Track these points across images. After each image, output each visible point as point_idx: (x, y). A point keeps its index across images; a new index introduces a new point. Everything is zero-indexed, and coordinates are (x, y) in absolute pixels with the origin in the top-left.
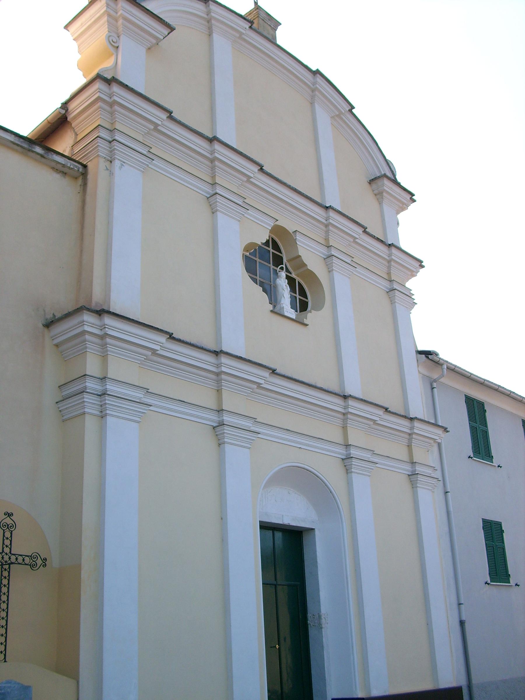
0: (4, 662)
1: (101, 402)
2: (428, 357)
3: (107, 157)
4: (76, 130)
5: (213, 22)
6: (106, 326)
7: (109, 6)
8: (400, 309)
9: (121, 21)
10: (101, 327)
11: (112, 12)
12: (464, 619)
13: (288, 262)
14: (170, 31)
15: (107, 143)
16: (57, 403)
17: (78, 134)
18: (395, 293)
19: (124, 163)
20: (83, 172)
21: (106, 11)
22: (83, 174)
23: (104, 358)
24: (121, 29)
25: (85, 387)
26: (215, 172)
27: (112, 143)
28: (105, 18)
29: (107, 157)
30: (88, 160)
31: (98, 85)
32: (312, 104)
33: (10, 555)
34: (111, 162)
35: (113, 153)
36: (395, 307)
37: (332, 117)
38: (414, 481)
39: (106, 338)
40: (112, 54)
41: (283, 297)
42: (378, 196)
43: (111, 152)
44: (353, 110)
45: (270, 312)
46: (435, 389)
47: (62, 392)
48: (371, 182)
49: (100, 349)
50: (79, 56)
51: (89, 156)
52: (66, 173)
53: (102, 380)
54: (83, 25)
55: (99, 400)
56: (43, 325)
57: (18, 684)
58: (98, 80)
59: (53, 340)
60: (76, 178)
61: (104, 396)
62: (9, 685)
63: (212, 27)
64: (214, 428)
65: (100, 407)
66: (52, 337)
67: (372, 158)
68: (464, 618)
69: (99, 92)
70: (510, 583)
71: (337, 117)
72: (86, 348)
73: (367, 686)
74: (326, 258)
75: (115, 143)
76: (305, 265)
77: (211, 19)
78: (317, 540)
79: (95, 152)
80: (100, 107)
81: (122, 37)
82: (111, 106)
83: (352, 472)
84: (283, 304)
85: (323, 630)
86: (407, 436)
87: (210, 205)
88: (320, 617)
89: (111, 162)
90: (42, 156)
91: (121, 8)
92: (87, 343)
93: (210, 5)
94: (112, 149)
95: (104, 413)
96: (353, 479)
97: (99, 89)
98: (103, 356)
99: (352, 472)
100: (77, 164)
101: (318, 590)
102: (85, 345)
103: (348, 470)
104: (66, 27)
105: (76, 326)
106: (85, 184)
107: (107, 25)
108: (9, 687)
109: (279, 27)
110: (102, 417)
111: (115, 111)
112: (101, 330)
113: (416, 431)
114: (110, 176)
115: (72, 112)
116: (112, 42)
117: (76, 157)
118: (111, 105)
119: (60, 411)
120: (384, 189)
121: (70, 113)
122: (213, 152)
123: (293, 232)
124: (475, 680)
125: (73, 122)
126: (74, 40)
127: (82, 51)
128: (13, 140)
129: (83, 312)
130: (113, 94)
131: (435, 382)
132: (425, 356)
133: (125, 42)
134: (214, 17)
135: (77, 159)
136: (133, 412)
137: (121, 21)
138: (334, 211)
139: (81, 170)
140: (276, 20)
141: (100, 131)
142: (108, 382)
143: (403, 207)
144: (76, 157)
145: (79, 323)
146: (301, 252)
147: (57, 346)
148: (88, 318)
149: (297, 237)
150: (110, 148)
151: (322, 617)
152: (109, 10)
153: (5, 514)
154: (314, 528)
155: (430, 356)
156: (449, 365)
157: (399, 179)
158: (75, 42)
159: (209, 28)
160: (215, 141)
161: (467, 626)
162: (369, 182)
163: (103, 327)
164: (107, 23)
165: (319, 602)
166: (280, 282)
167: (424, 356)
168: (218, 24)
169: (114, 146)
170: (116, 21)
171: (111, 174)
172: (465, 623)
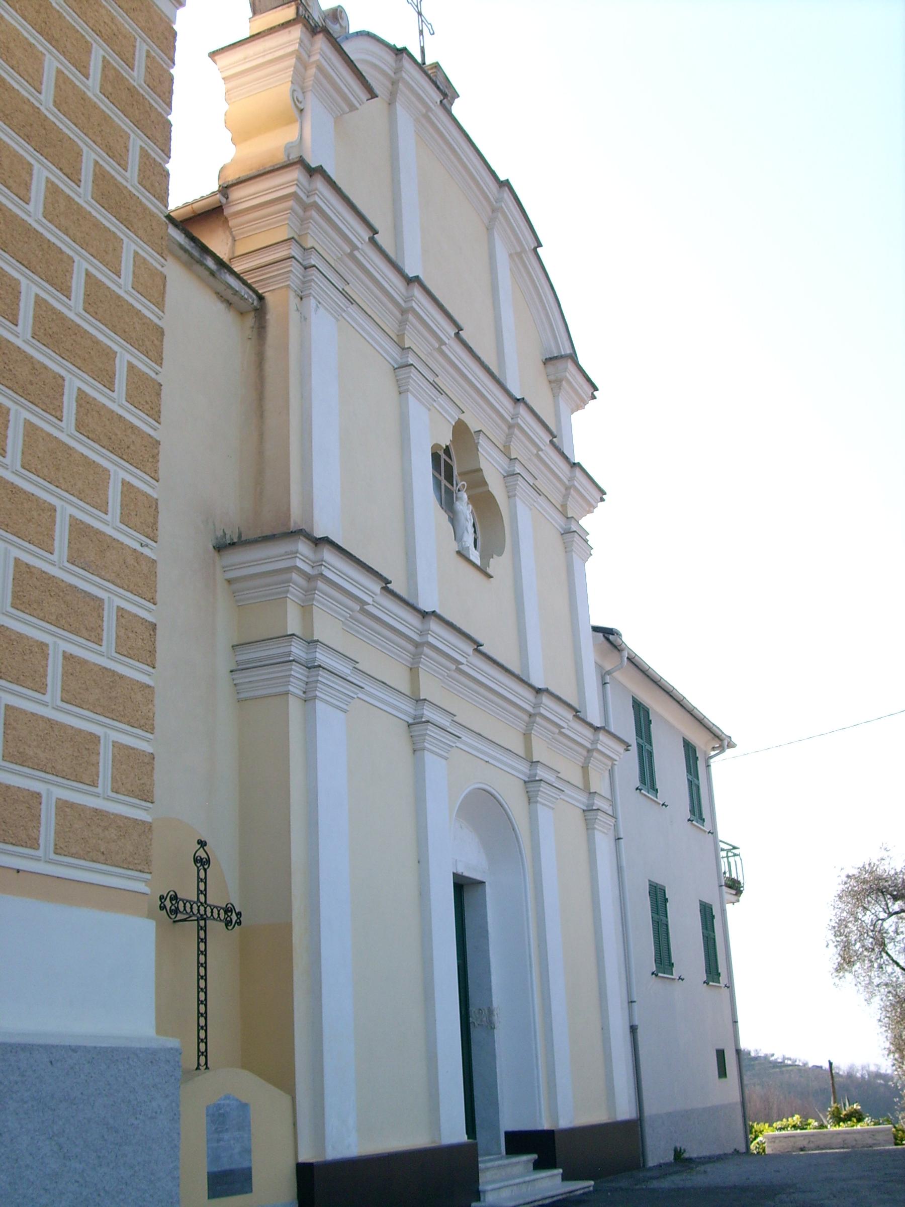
0: (205, 1069)
1: (308, 677)
2: (608, 639)
3: (298, 290)
5: (401, 85)
6: (324, 563)
7: (302, 45)
8: (576, 559)
9: (313, 71)
10: (314, 562)
11: (305, 56)
12: (637, 1024)
13: (459, 475)
14: (370, 97)
15: (300, 268)
16: (232, 671)
17: (237, 238)
18: (574, 537)
19: (320, 303)
21: (297, 50)
22: (256, 310)
23: (306, 610)
24: (309, 82)
25: (289, 654)
26: (405, 329)
27: (308, 270)
28: (293, 61)
29: (298, 290)
30: (264, 288)
31: (296, 174)
32: (489, 229)
33: (206, 906)
34: (301, 299)
35: (307, 285)
36: (572, 556)
37: (510, 255)
38: (590, 819)
39: (318, 580)
40: (297, 121)
41: (466, 532)
42: (553, 385)
43: (303, 283)
44: (539, 250)
45: (455, 553)
46: (608, 685)
47: (236, 655)
48: (548, 361)
49: (302, 595)
50: (225, 107)
51: (268, 283)
52: (230, 304)
53: (309, 643)
55: (306, 673)
56: (214, 547)
57: (237, 1100)
58: (298, 166)
59: (225, 571)
60: (242, 314)
61: (317, 669)
62: (228, 1102)
63: (397, 94)
64: (409, 725)
65: (305, 686)
66: (223, 568)
67: (551, 325)
68: (636, 1022)
69: (297, 184)
70: (672, 974)
71: (517, 256)
72: (288, 591)
73: (554, 1113)
74: (508, 476)
75: (313, 271)
76: (485, 483)
77: (398, 81)
78: (488, 899)
79: (283, 279)
80: (291, 208)
81: (309, 95)
82: (305, 208)
83: (537, 802)
84: (465, 542)
85: (495, 1031)
86: (585, 753)
87: (397, 381)
88: (491, 1012)
89: (301, 299)
90: (212, 273)
92: (291, 584)
93: (403, 60)
94: (306, 279)
95: (310, 695)
96: (539, 812)
97: (297, 180)
98: (303, 607)
99: (537, 802)
100: (251, 293)
101: (488, 972)
102: (287, 588)
103: (531, 799)
104: (213, 55)
105: (280, 556)
106: (261, 327)
107: (292, 72)
108: (229, 1105)
109: (456, 101)
110: (305, 701)
111: (311, 218)
112: (313, 567)
113: (599, 747)
114: (301, 322)
115: (234, 203)
116: (295, 99)
118: (306, 207)
119: (235, 684)
120: (566, 376)
121: (231, 204)
122: (408, 299)
123: (475, 432)
124: (648, 1111)
125: (232, 219)
126: (223, 79)
127: (233, 100)
128: (183, 243)
129: (299, 538)
130: (314, 192)
131: (609, 675)
132: (604, 636)
133: (311, 103)
134: (404, 79)
135: (249, 282)
136: (343, 697)
137: (313, 71)
138: (526, 409)
139: (255, 303)
140: (454, 89)
141: (291, 247)
142: (319, 648)
143: (580, 404)
145: (287, 553)
146: (483, 465)
147: (229, 581)
148: (303, 547)
149: (480, 441)
150: (304, 277)
151: (495, 1013)
152: (301, 50)
153: (198, 843)
154: (484, 881)
155: (611, 637)
156: (631, 652)
157: (582, 362)
158: (223, 81)
159: (391, 93)
160: (416, 283)
161: (640, 1032)
162: (544, 360)
163: (321, 563)
164: (292, 69)
165: (490, 989)
166: (461, 507)
167: (601, 635)
170: (306, 68)
171: (303, 318)
172: (637, 1029)
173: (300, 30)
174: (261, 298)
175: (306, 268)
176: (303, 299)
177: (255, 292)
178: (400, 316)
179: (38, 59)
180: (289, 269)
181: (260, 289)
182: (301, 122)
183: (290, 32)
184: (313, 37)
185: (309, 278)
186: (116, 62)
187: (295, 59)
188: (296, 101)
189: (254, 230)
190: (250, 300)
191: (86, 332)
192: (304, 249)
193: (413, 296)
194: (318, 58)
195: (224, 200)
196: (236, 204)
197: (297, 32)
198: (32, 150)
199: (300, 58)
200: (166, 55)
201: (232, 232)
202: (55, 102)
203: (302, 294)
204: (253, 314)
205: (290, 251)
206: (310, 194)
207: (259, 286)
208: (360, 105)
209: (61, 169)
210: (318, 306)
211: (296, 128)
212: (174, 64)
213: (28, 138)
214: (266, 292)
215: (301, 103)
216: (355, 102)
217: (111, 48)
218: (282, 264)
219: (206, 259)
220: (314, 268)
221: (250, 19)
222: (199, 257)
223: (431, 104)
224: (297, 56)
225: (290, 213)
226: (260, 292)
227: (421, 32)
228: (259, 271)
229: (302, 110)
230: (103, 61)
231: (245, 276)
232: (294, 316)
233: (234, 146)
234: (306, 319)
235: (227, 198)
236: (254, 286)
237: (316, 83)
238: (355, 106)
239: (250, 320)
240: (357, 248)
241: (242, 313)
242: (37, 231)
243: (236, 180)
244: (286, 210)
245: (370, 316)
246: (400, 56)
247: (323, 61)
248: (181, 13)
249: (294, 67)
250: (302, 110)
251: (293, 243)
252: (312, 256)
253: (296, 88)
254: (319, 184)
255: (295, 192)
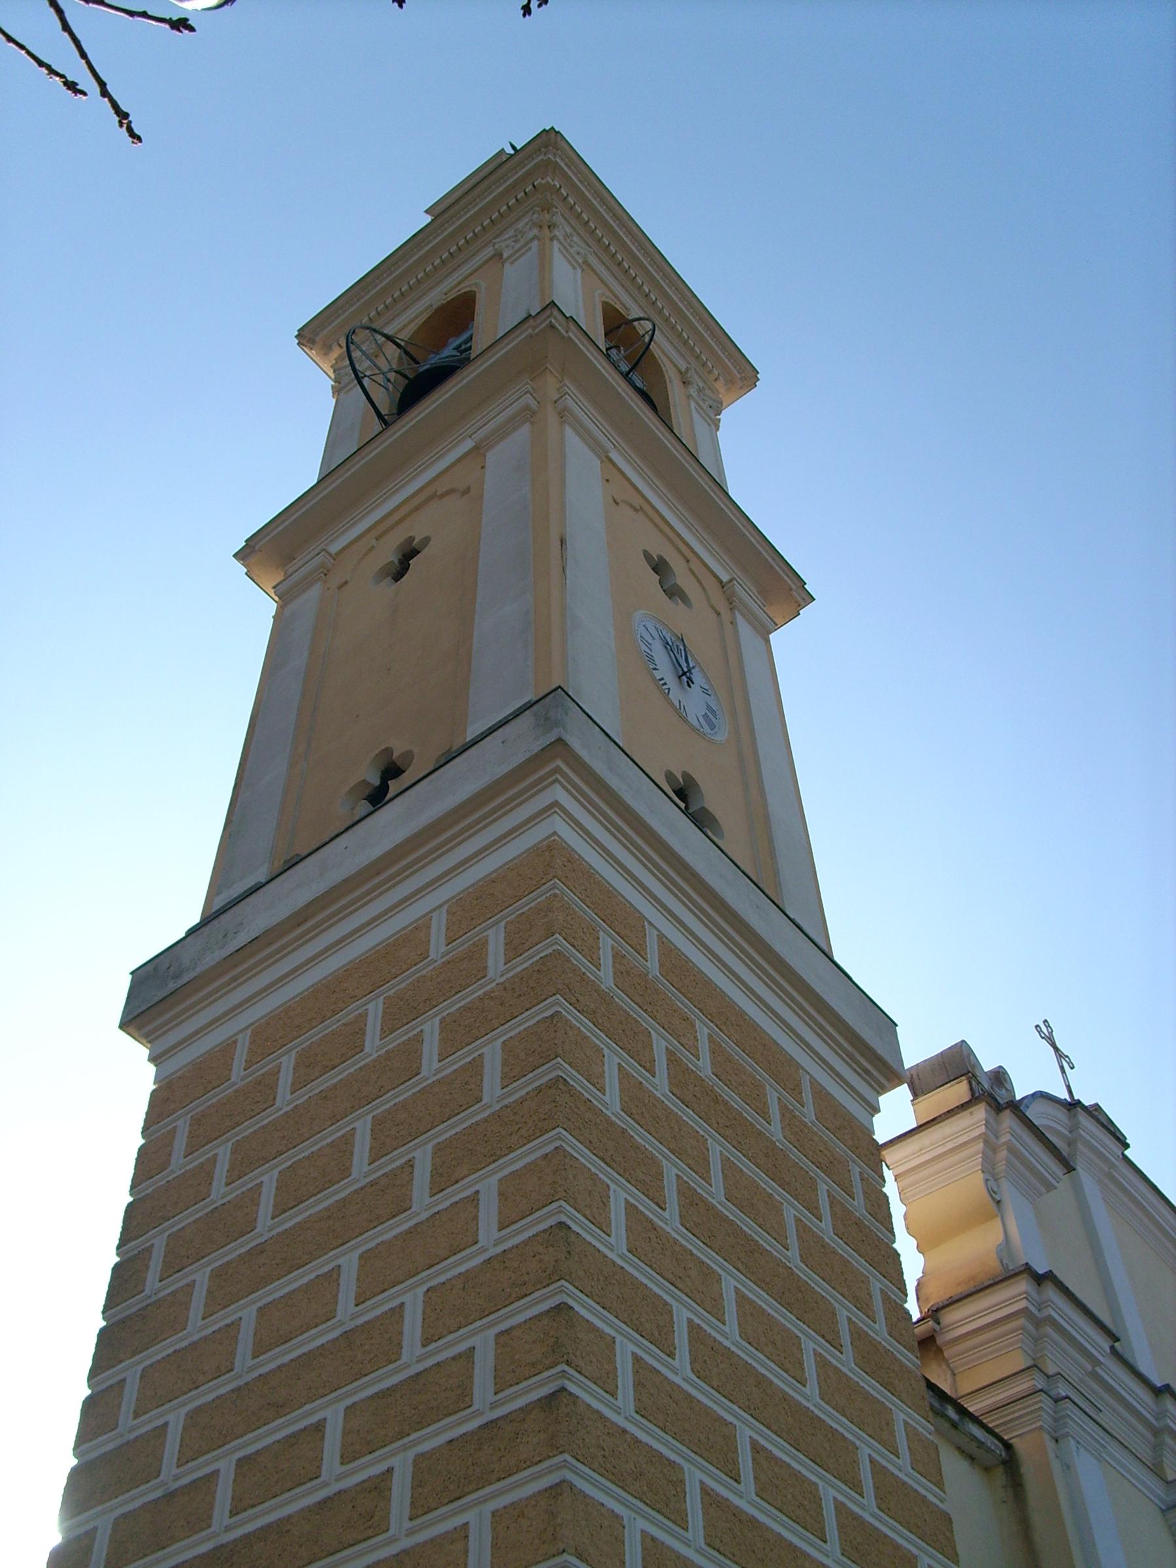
4: (951, 1365)
5: (1080, 1145)
14: (1066, 1171)
17: (955, 1372)
20: (1007, 1459)
22: (1004, 1463)
24: (1001, 1167)
28: (980, 1146)
31: (1023, 1285)
40: (997, 1216)
43: (1056, 1420)
54: (923, 1152)
58: (1024, 1275)
80: (1023, 1328)
81: (1004, 1184)
82: (1037, 1325)
89: (1057, 1441)
90: (954, 1425)
91: (1008, 1130)
97: (1026, 1293)
107: (981, 1159)
117: (990, 1419)
118: (1038, 1323)
133: (1008, 1192)
135: (990, 1425)
137: (1003, 1154)
144: (990, 1419)
150: (1055, 1412)
152: (989, 1133)
168: (1085, 1150)
169: (1066, 1409)
170: (995, 1150)
173: (984, 1108)
174: (1008, 1446)
175: (1056, 1401)
176: (1060, 1441)
177: (1001, 1440)
178: (1153, 1438)
179: (777, 1209)
180: (1037, 1406)
181: (1006, 1434)
182: (1002, 1217)
183: (971, 1113)
184: (998, 1114)
185: (1063, 1413)
186: (840, 1194)
187: (982, 1144)
188: (992, 1192)
189: (978, 1358)
190: (998, 1452)
191: (886, 1536)
192: (1048, 1377)
193: (1167, 1411)
194: (1008, 1138)
195: (937, 1327)
196: (950, 1330)
197: (980, 1113)
198: (795, 1319)
199: (987, 1142)
200: (875, 1173)
201: (949, 1364)
202: (801, 1256)
203: (1057, 1435)
204: (1001, 1469)
205: (1034, 1382)
206: (1043, 1306)
207: (1004, 1430)
208: (1058, 1182)
209: (823, 1337)
210: (1078, 1448)
211: (997, 1223)
212: (884, 1181)
213: (789, 1306)
214: (1014, 1437)
215: (995, 1193)
216: (1053, 1181)
217: (831, 1179)
218: (1029, 1401)
219: (947, 1409)
220: (1067, 1400)
221: (912, 1101)
222: (939, 1407)
223: (1113, 1160)
224: (984, 1139)
225: (1021, 1334)
226: (1006, 1438)
227: (1062, 1068)
228: (995, 1414)
229: (998, 1202)
230: (828, 1196)
231: (986, 1418)
232: (1056, 1465)
233: (921, 1255)
234: (1068, 1467)
235: (939, 1324)
236: (997, 1430)
237: (986, 1162)
238: (1053, 1185)
239: (1000, 1476)
240: (1099, 1363)
241: (987, 1469)
242: (820, 1418)
243: (948, 1300)
244: (1017, 1330)
245: (1126, 1447)
246: (1073, 1112)
247: (1015, 1141)
248: (876, 1119)
249: (983, 1153)
250: (998, 1202)
251: (1035, 1371)
252: (1059, 1384)
253: (990, 1178)
254: (1051, 1293)
255: (1027, 1308)
